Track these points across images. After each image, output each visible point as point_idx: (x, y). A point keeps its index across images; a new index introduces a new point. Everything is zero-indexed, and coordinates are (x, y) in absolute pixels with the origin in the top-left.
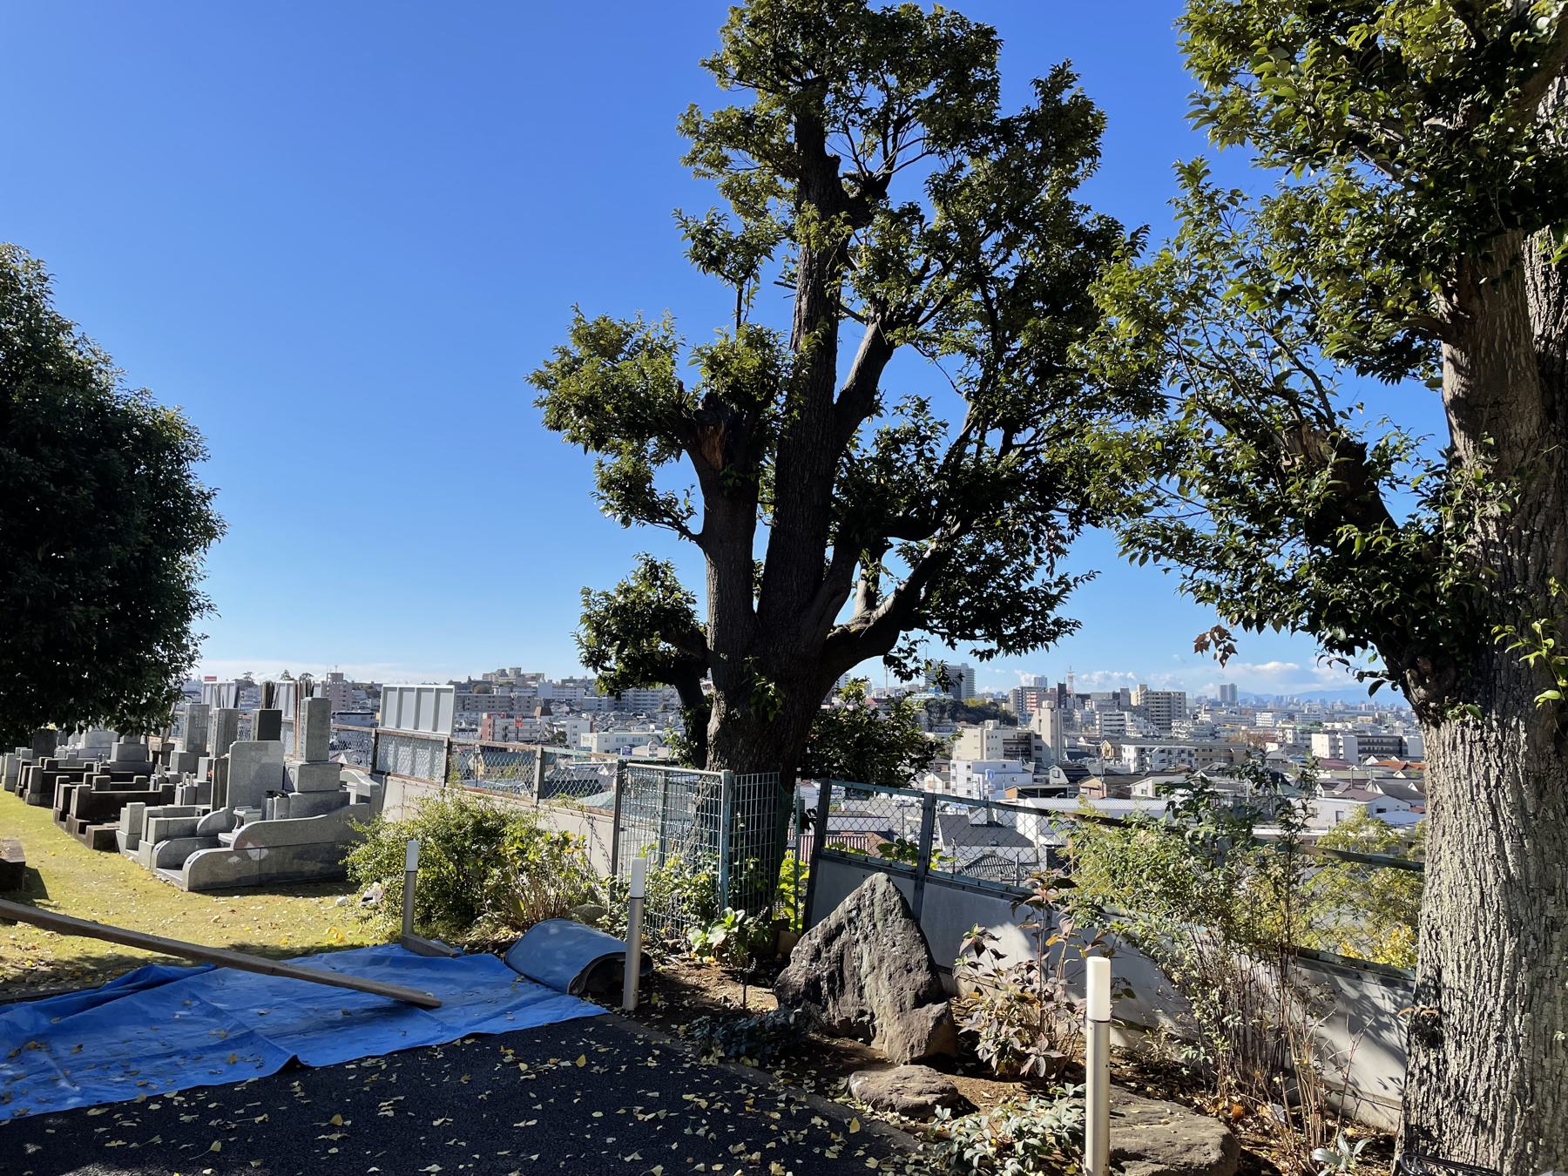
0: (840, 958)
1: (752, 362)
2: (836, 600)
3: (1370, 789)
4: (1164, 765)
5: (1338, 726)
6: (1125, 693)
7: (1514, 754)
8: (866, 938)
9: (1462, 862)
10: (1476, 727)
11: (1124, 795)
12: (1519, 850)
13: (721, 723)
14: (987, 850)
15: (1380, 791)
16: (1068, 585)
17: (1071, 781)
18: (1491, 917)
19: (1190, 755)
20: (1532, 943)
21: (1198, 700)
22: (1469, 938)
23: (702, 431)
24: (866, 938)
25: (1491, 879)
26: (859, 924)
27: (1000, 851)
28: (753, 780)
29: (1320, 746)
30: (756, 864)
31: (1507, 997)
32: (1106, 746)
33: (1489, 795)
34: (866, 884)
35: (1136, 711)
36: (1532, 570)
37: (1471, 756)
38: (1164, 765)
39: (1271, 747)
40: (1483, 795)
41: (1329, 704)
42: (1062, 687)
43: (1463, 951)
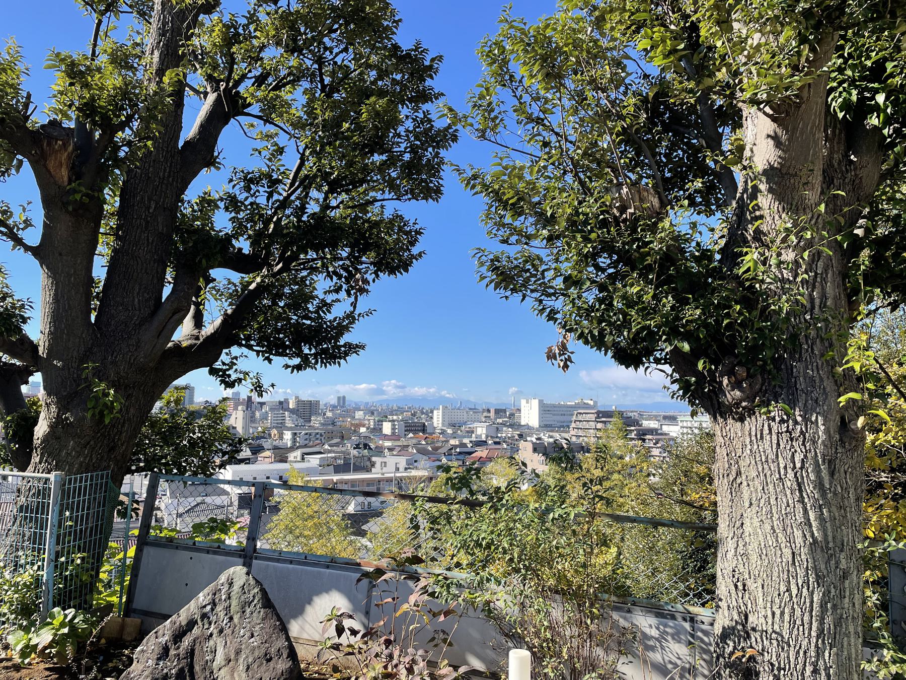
0: (191, 653)
1: (112, 80)
2: (177, 317)
3: (410, 450)
4: (307, 442)
5: (395, 417)
6: (287, 401)
7: (814, 442)
8: (221, 631)
9: (773, 527)
10: (782, 421)
11: (284, 460)
12: (821, 518)
13: (51, 426)
14: (199, 499)
16: (354, 318)
17: (253, 454)
18: (801, 573)
19: (321, 435)
20: (833, 590)
21: (325, 405)
22: (783, 588)
24: (221, 631)
25: (799, 540)
26: (213, 618)
27: (208, 500)
28: (84, 480)
29: (387, 428)
30: (83, 559)
31: (818, 637)
32: (274, 432)
33: (796, 474)
34: (223, 578)
35: (292, 411)
36: (817, 302)
37: (778, 444)
38: (307, 442)
40: (791, 474)
43: (777, 600)
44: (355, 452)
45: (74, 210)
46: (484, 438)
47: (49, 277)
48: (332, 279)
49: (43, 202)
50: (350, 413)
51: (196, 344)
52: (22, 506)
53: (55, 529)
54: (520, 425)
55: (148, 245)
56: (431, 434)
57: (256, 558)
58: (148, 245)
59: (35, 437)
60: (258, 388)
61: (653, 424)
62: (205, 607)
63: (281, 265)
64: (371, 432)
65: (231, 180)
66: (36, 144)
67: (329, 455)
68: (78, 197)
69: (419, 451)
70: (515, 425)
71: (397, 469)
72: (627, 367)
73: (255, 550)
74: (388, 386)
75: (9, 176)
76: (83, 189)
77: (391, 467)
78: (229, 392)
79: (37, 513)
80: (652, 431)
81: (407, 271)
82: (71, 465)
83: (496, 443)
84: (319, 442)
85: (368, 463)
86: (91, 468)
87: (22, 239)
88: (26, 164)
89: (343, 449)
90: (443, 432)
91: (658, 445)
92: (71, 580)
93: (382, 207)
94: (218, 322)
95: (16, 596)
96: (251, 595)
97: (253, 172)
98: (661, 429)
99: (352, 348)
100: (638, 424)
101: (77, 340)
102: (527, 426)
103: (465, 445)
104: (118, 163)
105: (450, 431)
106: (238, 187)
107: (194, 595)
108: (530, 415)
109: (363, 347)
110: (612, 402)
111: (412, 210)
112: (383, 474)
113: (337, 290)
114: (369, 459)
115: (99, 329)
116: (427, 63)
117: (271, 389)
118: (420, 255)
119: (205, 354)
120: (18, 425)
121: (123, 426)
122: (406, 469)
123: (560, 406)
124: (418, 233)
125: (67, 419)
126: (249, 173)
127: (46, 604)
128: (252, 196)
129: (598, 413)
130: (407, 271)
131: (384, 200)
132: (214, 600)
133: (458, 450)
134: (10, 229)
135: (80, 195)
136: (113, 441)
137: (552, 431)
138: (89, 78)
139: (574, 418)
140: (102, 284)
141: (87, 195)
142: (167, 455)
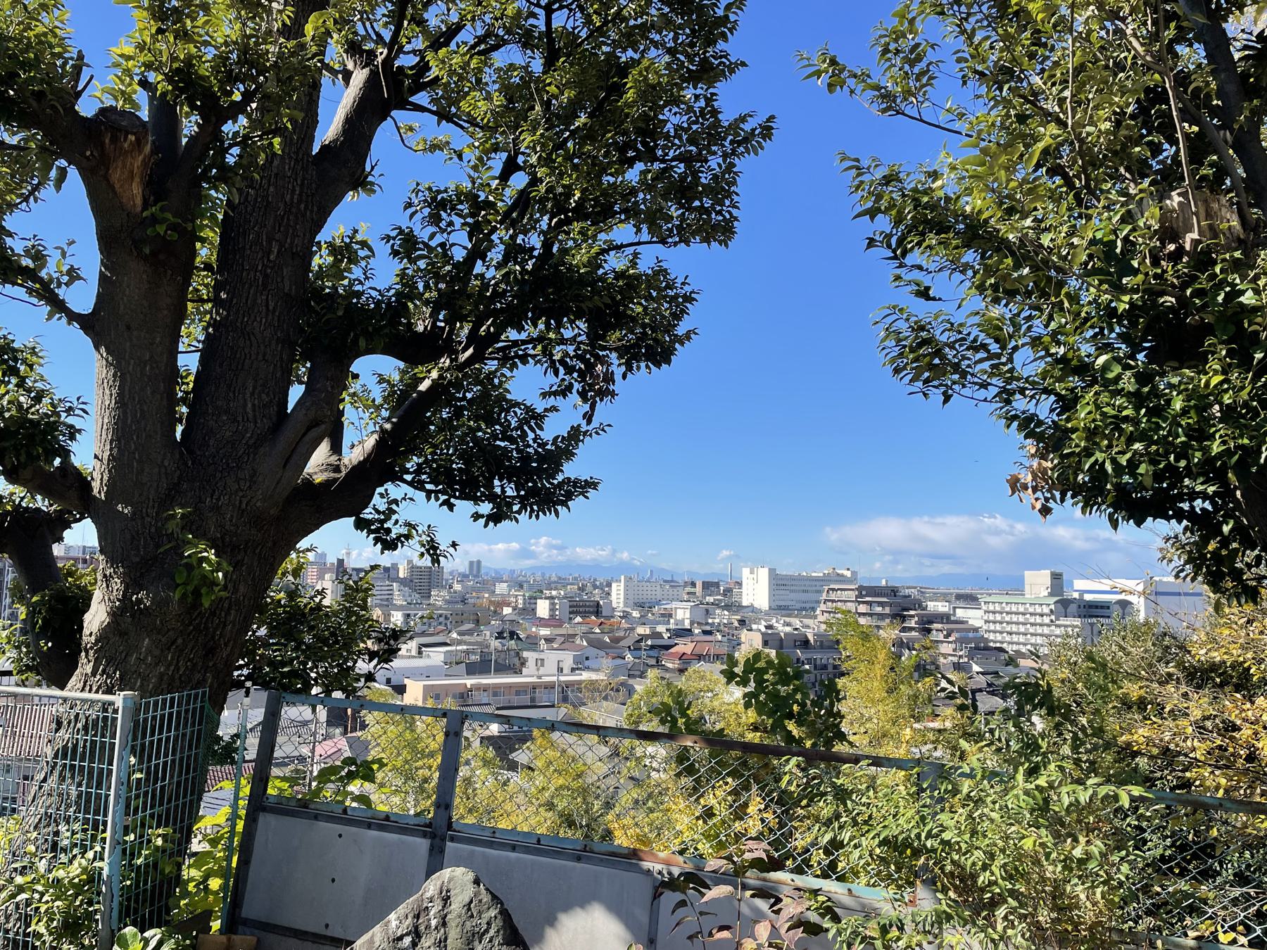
3: (578, 641)
4: (425, 628)
5: (554, 593)
19: (446, 618)
21: (451, 573)
23: (114, 140)
28: (167, 705)
29: (543, 609)
35: (403, 582)
38: (425, 628)
39: (507, 611)
41: (547, 576)
42: (341, 562)
44: (495, 644)
45: (154, 254)
46: (687, 625)
47: (109, 364)
48: (556, 373)
49: (101, 237)
50: (488, 585)
51: (335, 480)
52: (65, 747)
53: (124, 788)
54: (740, 607)
55: (267, 315)
57: (452, 839)
58: (267, 315)
59: (86, 632)
60: (432, 549)
61: (941, 607)
62: (401, 938)
63: (471, 351)
64: (520, 614)
65: (409, 205)
66: (90, 144)
67: (459, 648)
68: (161, 229)
69: (591, 643)
70: (733, 607)
71: (560, 670)
72: (1139, 523)
73: (450, 826)
75: (36, 201)
76: (169, 216)
77: (550, 667)
78: (387, 559)
79: (92, 761)
80: (944, 618)
81: (668, 362)
82: (145, 679)
83: (705, 632)
84: (442, 627)
85: (516, 661)
86: (177, 683)
87: (63, 302)
88: (73, 174)
89: (479, 639)
90: (626, 616)
91: (950, 639)
92: (146, 873)
93: (636, 255)
94: (371, 442)
95: (58, 903)
96: (484, 921)
97: (446, 191)
98: (954, 614)
99: (585, 486)
100: (920, 606)
101: (157, 470)
102: (752, 608)
103: (659, 635)
104: (226, 174)
105: (636, 614)
106: (419, 216)
107: (381, 915)
108: (756, 591)
109: (592, 485)
110: (880, 573)
111: (685, 262)
112: (540, 677)
113: (564, 391)
115: (191, 452)
116: (720, 12)
117: (451, 550)
118: (688, 336)
119: (347, 496)
120: (51, 610)
121: (228, 613)
122: (573, 670)
123: (801, 578)
124: (689, 299)
125: (139, 601)
126: (439, 192)
127: (107, 918)
128: (443, 231)
129: (860, 589)
130: (668, 362)
131: (639, 243)
132: (416, 927)
133: (649, 642)
134: (45, 285)
135: (164, 227)
136: (213, 637)
137: (789, 616)
138: (188, 22)
139: (824, 596)
140: (192, 378)
141: (173, 227)
142: (292, 660)
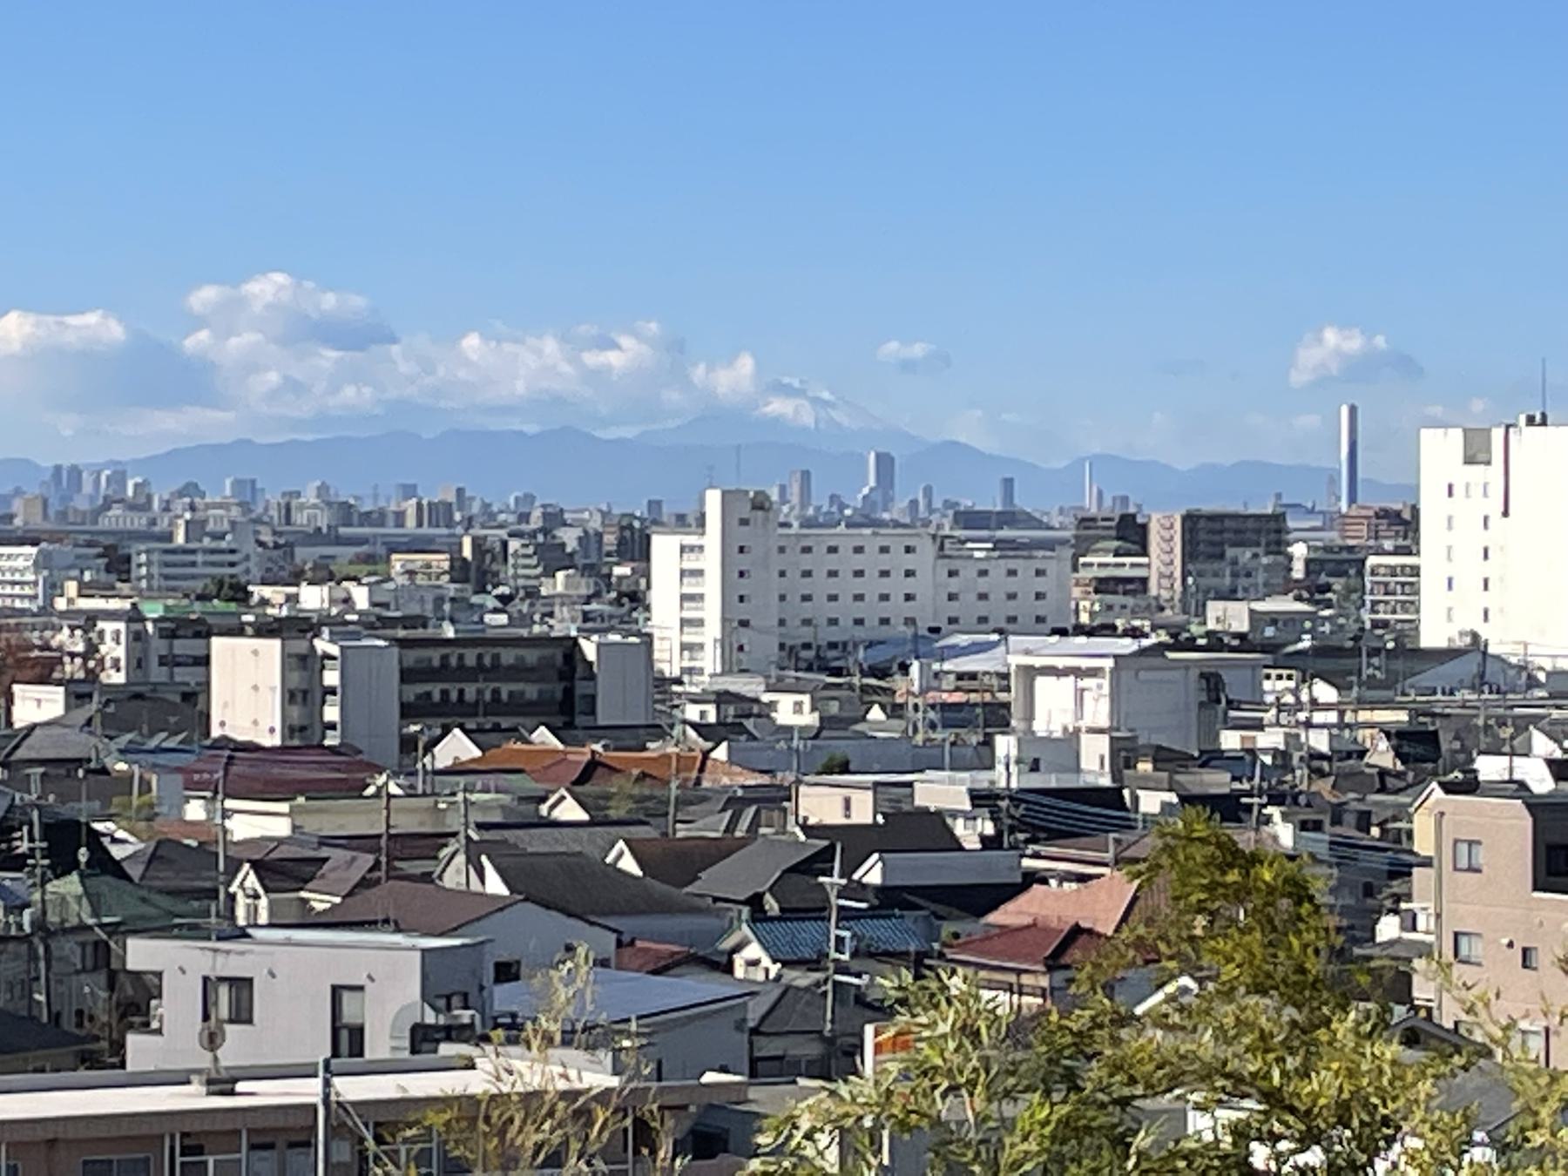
3: (455, 876)
5: (313, 598)
15: (495, 885)
29: (245, 690)
54: (1410, 654)
56: (634, 735)
64: (112, 725)
70: (1374, 656)
71: (348, 1041)
74: (226, 318)
77: (289, 1023)
85: (92, 990)
90: (737, 720)
103: (932, 830)
105: (794, 711)
112: (222, 1084)
114: (102, 958)
133: (872, 873)
